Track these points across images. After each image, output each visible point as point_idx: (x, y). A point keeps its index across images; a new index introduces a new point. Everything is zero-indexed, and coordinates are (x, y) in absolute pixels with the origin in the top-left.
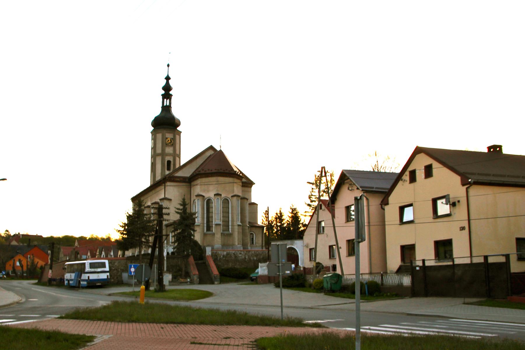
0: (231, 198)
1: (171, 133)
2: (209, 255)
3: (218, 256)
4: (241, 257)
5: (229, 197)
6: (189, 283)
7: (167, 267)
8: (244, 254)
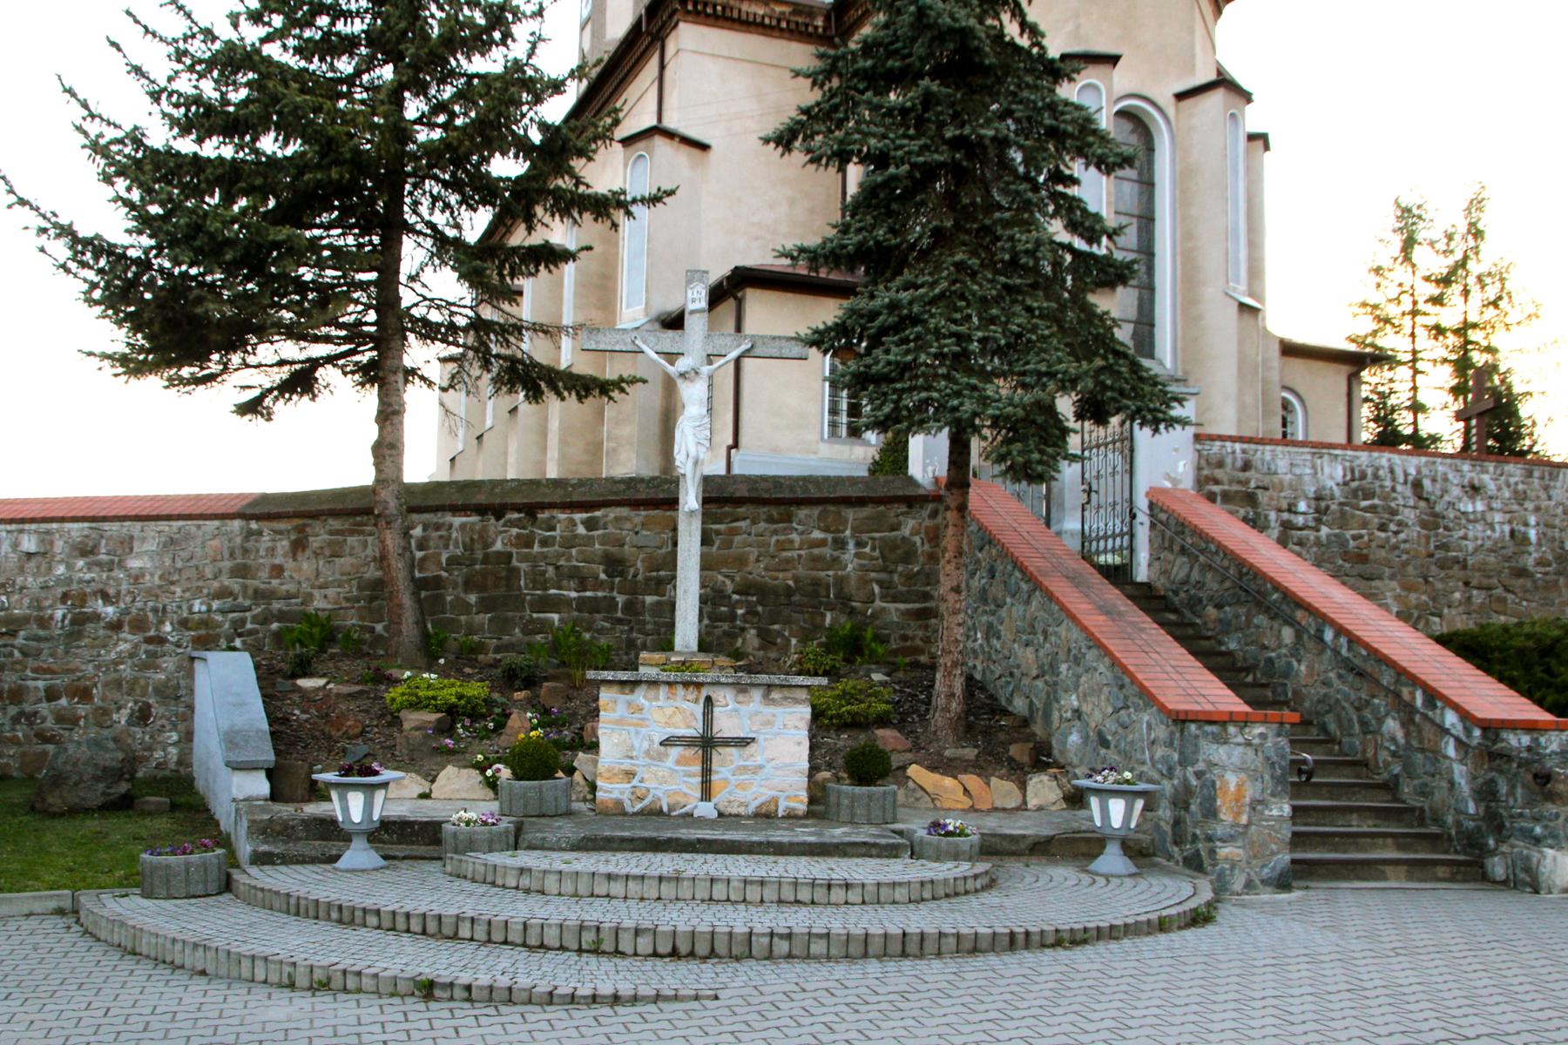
0: (1171, 112)
1: (676, 25)
2: (1174, 481)
3: (1262, 497)
4: (1476, 530)
5: (1161, 102)
6: (1112, 860)
7: (711, 600)
8: (1507, 494)
